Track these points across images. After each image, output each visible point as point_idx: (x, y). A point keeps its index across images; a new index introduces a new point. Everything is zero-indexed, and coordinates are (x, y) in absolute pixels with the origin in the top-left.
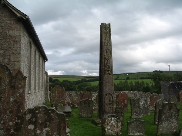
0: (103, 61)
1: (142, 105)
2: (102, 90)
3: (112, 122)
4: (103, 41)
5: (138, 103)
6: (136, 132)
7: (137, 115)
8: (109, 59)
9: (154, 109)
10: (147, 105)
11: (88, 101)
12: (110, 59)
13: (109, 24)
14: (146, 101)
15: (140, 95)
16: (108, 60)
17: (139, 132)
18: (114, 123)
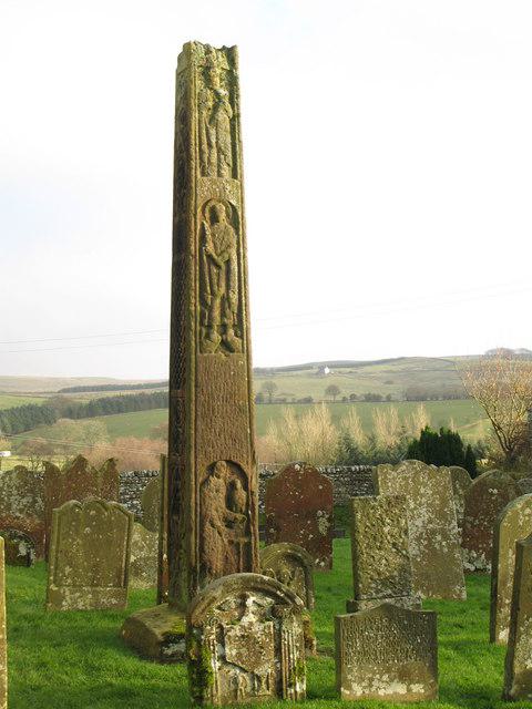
0: (194, 270)
1: (418, 539)
2: (185, 442)
3: (245, 620)
4: (194, 150)
5: (396, 521)
6: (385, 677)
7: (390, 592)
8: (228, 263)
9: (490, 567)
10: (445, 537)
11: (98, 511)
12: (234, 257)
13: (230, 54)
14: (442, 515)
15: (405, 479)
16: (218, 267)
17: (404, 676)
18: (258, 628)
